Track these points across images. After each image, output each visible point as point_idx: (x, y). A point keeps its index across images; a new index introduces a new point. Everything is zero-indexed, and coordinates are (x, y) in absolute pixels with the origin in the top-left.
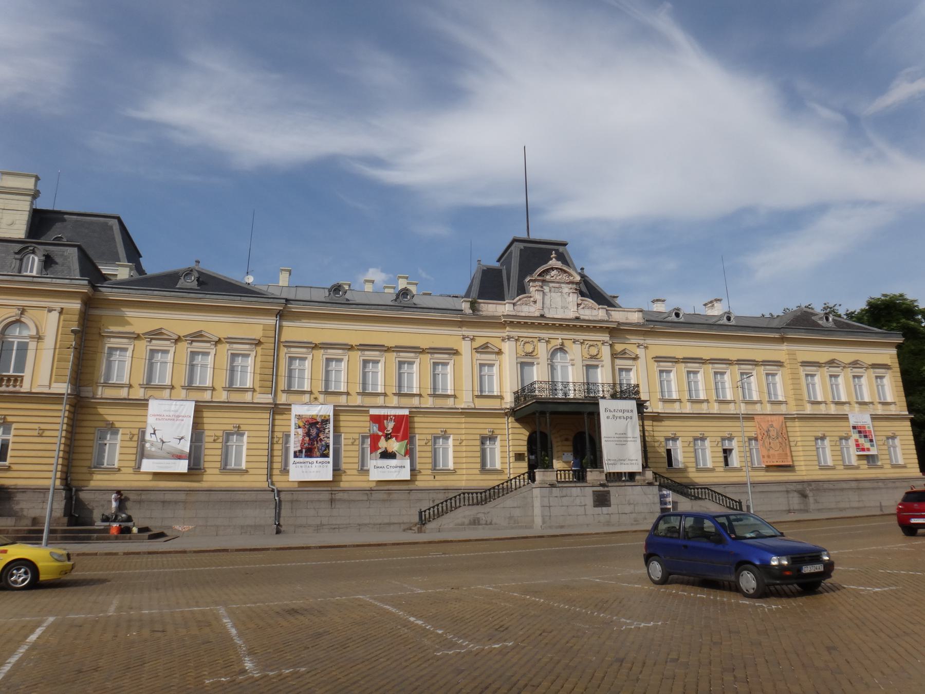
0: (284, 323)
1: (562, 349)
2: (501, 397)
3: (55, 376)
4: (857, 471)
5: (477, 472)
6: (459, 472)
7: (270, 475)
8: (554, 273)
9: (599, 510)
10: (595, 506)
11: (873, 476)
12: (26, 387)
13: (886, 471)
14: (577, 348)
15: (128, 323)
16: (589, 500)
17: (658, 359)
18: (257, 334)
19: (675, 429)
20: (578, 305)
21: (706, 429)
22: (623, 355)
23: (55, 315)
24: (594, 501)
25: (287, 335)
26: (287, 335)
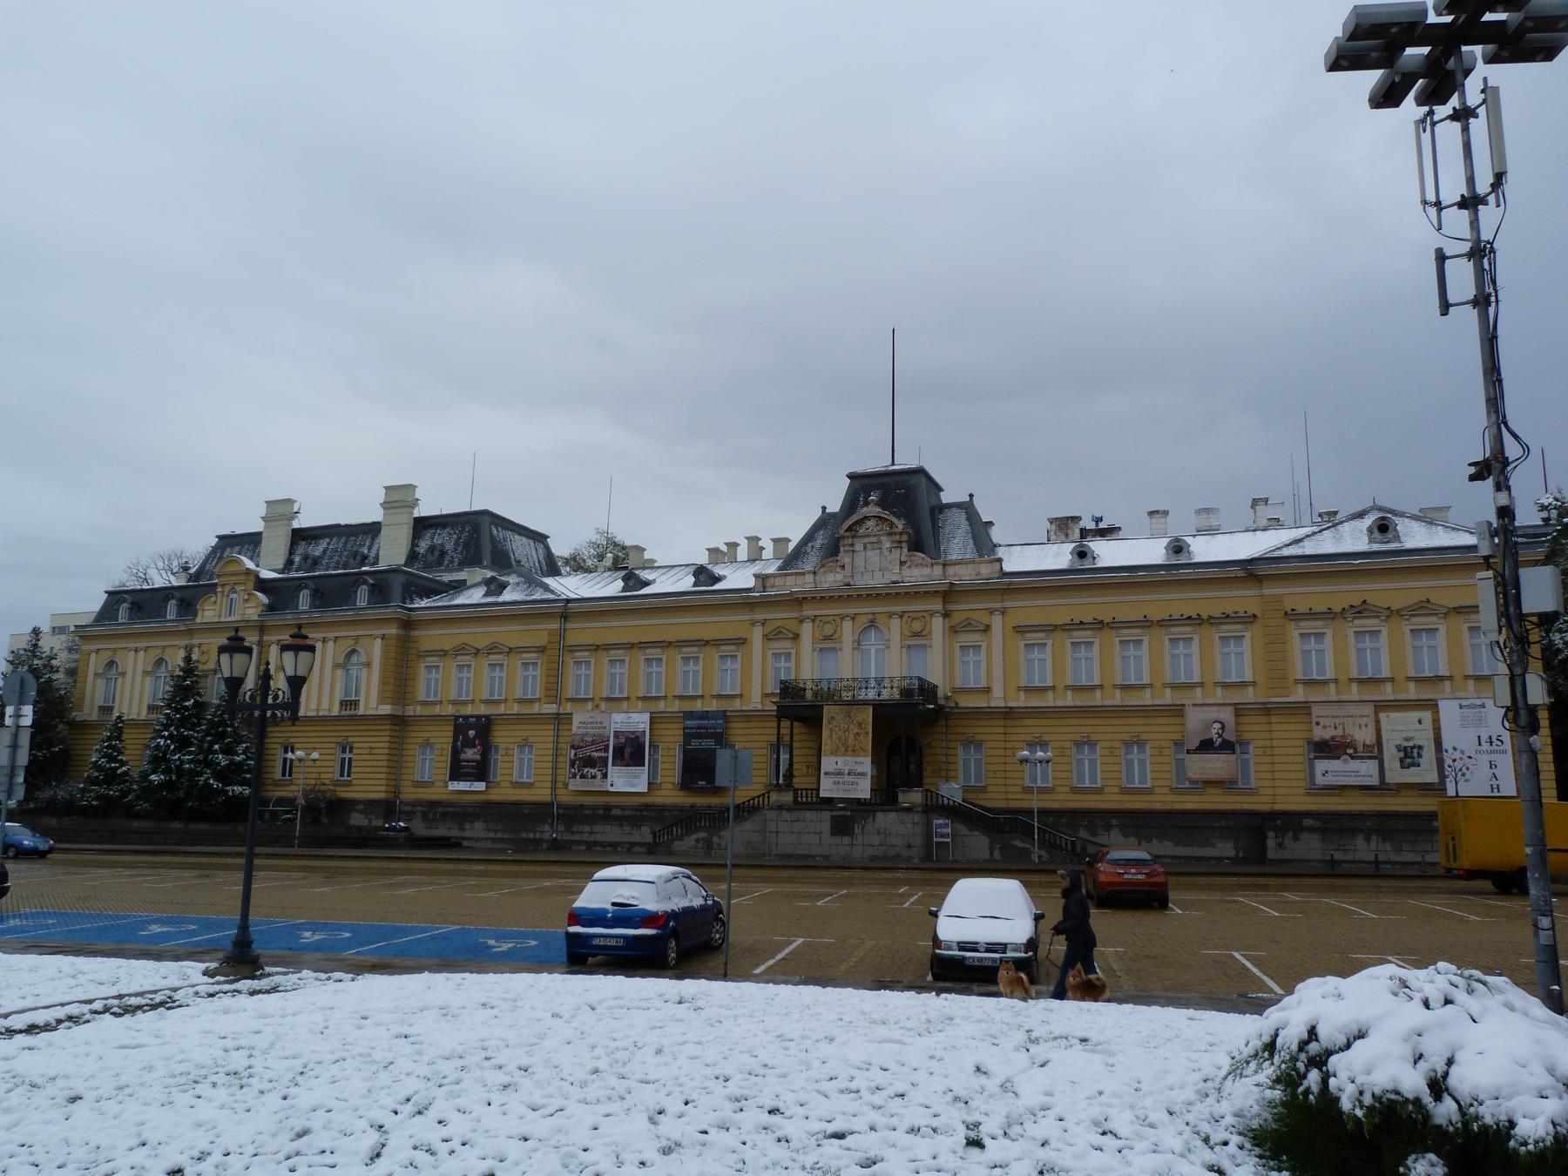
0: (568, 626)
1: (872, 624)
2: (988, 690)
3: (381, 701)
4: (1149, 798)
5: (1302, 791)
6: (1107, 790)
7: (554, 788)
8: (870, 523)
9: (837, 840)
10: (833, 834)
11: (1378, 808)
12: (361, 711)
13: (1061, 797)
14: (895, 623)
15: (1397, 538)
16: (826, 827)
17: (1020, 630)
18: (542, 640)
19: (1090, 729)
20: (902, 563)
21: (1048, 730)
22: (968, 626)
23: (379, 641)
24: (832, 828)
25: (572, 639)
26: (572, 639)
